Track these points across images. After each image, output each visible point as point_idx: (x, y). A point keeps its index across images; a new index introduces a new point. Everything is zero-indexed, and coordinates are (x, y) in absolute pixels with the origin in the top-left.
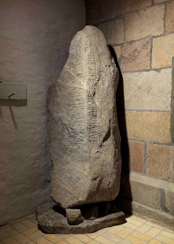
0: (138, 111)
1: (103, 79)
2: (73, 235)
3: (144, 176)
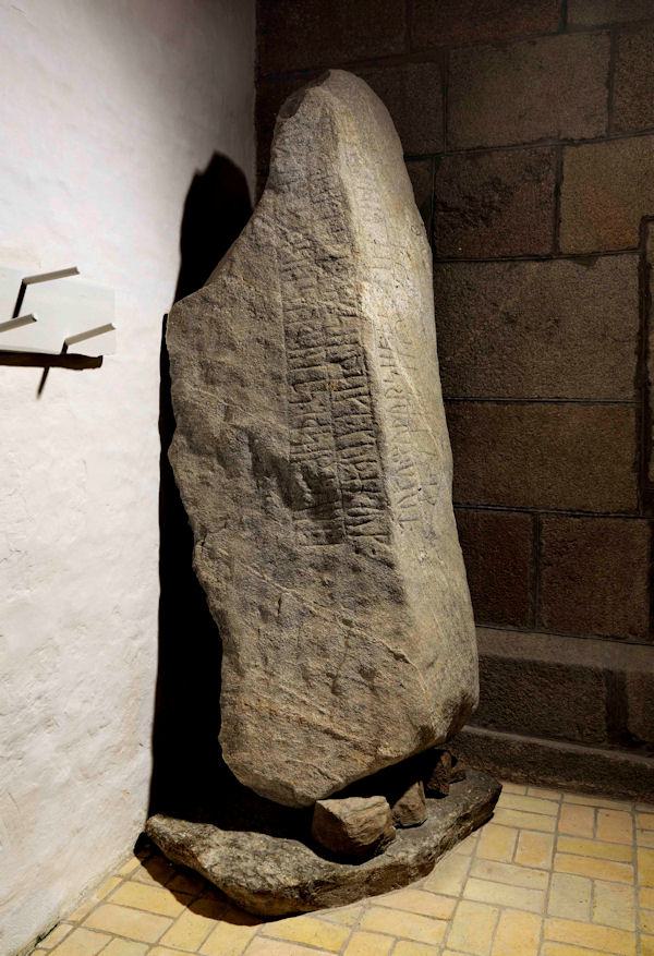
0: (506, 403)
2: (373, 900)
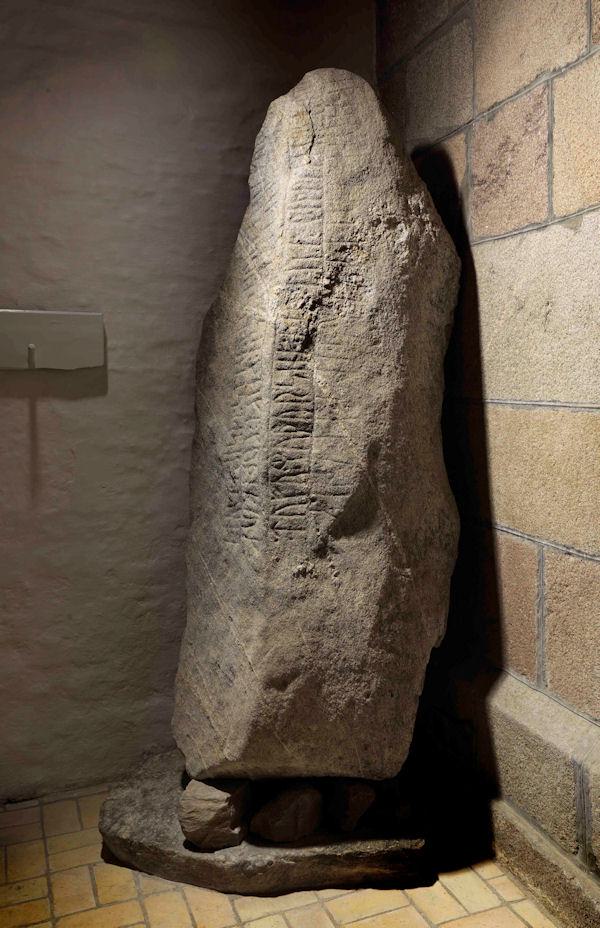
1: (354, 278)
3: (537, 695)
